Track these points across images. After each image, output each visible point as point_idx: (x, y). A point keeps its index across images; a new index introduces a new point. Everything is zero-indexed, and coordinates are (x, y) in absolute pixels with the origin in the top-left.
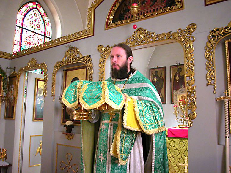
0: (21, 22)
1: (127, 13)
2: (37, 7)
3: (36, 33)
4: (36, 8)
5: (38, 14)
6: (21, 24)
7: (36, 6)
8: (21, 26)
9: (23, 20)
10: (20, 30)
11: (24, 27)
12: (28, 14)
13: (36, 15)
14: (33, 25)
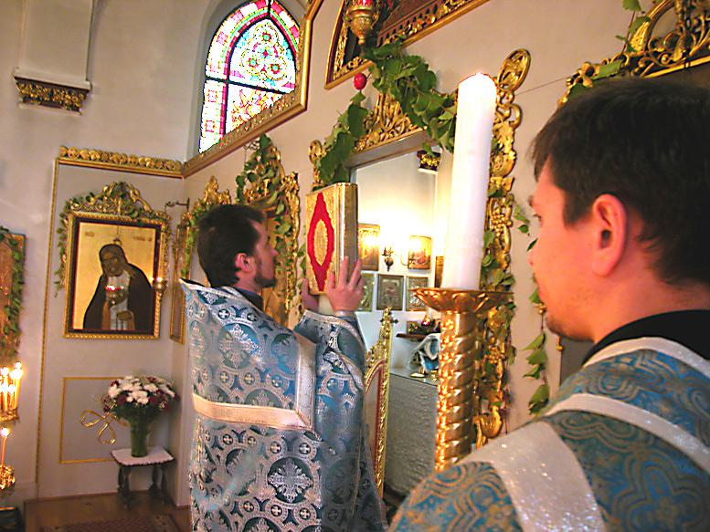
0: (223, 65)
1: (385, 23)
2: (269, 13)
3: (267, 90)
4: (267, 16)
5: (273, 31)
6: (222, 71)
7: (266, 10)
8: (225, 77)
9: (229, 60)
10: (221, 89)
11: (232, 78)
12: (242, 40)
13: (267, 37)
14: (258, 69)
